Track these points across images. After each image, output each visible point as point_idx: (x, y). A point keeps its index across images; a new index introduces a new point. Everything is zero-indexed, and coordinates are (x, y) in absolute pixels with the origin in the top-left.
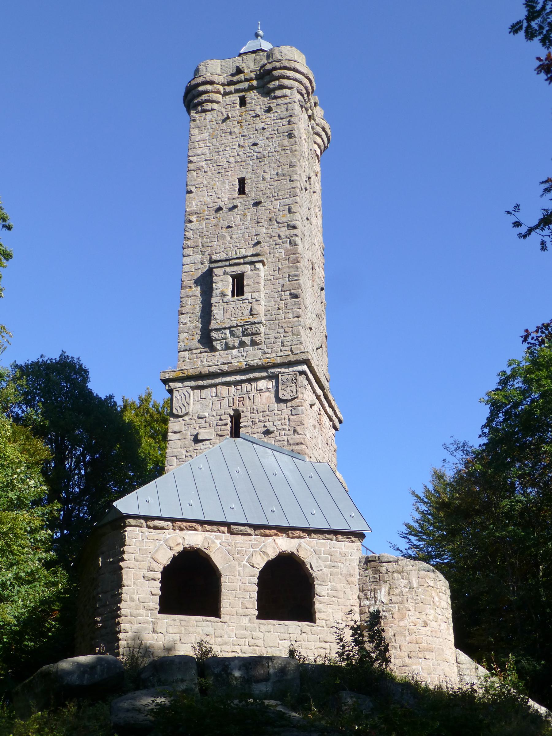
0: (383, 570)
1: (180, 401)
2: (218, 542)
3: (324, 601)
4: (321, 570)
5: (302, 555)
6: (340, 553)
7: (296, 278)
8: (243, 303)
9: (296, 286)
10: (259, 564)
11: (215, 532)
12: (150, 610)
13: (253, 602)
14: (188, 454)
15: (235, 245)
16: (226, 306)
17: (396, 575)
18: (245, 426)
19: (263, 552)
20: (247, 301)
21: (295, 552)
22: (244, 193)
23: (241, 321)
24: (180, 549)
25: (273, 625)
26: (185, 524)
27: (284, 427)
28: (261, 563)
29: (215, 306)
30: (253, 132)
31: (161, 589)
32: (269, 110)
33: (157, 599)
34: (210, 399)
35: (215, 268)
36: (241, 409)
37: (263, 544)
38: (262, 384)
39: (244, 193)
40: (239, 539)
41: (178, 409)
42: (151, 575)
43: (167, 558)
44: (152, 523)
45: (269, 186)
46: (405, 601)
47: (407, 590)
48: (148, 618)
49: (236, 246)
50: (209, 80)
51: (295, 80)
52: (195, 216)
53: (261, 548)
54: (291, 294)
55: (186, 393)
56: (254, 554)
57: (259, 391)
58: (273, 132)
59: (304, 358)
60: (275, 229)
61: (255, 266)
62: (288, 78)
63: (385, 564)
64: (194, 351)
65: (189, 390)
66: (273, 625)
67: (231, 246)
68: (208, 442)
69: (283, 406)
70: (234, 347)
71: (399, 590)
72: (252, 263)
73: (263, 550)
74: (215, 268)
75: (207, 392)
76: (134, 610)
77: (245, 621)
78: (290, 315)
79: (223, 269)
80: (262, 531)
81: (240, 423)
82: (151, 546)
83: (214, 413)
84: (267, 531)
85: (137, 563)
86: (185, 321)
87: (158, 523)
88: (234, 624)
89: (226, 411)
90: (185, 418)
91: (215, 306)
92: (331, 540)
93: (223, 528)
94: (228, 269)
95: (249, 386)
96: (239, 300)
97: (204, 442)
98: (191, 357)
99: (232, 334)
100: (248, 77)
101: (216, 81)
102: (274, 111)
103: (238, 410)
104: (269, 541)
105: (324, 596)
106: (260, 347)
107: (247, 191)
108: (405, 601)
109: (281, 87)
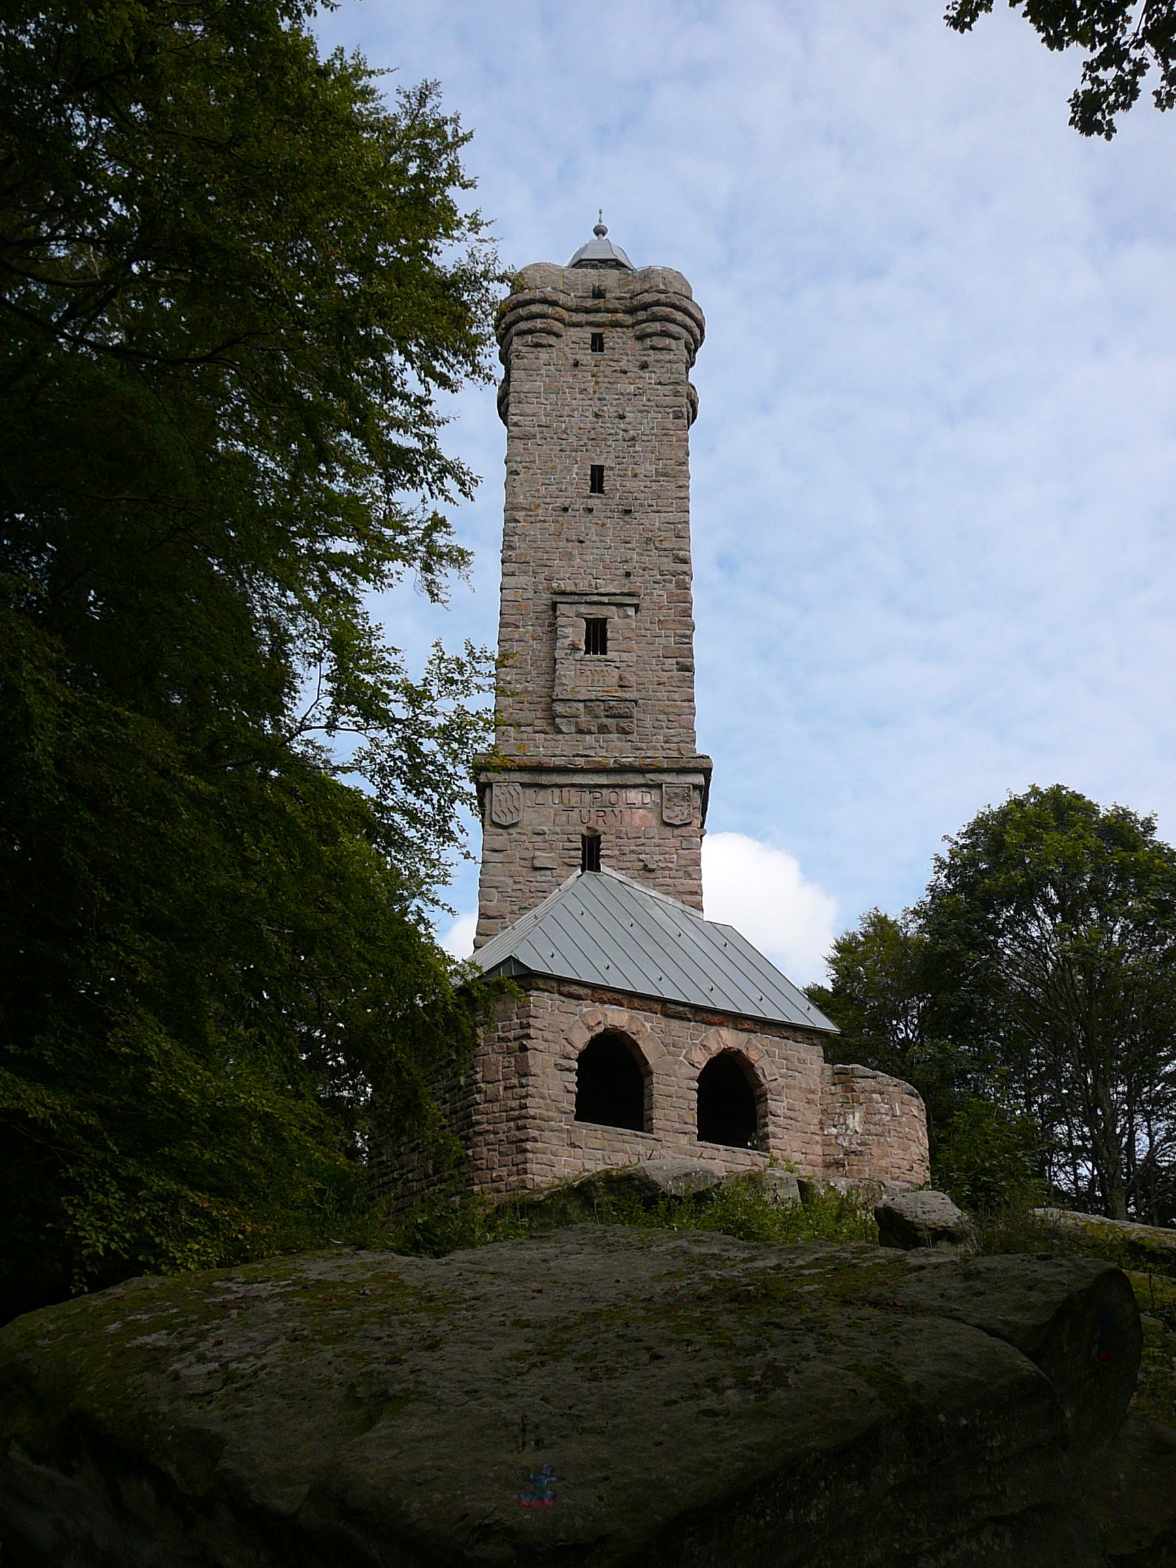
0: (857, 1086)
1: (503, 803)
2: (648, 1025)
3: (779, 1123)
4: (776, 1079)
5: (753, 1056)
6: (798, 1059)
7: (687, 641)
8: (606, 665)
9: (686, 652)
10: (700, 1063)
11: (644, 1010)
12: (565, 1113)
13: (693, 1115)
14: (518, 887)
15: (588, 571)
16: (579, 667)
17: (874, 1095)
18: (607, 856)
19: (704, 1046)
20: (613, 664)
21: (744, 1051)
22: (602, 491)
23: (604, 694)
24: (600, 1029)
25: (718, 1150)
26: (609, 995)
27: (670, 865)
28: (702, 1059)
29: (561, 663)
30: (617, 397)
31: (577, 1084)
32: (644, 366)
33: (573, 1097)
34: (552, 807)
35: (561, 603)
36: (600, 829)
37: (704, 1034)
38: (634, 796)
39: (602, 491)
40: (675, 1024)
41: (500, 814)
42: (565, 1063)
43: (585, 1041)
44: (566, 989)
45: (642, 488)
46: (887, 1134)
47: (889, 1118)
48: (562, 1124)
49: (590, 574)
50: (550, 299)
51: (685, 327)
52: (523, 513)
53: (702, 1040)
54: (677, 663)
55: (513, 792)
56: (693, 1047)
57: (631, 806)
58: (648, 403)
59: (705, 766)
60: (653, 558)
61: (625, 611)
62: (674, 321)
63: (859, 1080)
64: (523, 729)
65: (519, 788)
66: (718, 1150)
67: (582, 571)
68: (548, 872)
69: (668, 832)
70: (590, 733)
71: (878, 1117)
72: (620, 605)
73: (704, 1043)
74: (561, 603)
75: (544, 796)
76: (544, 1112)
77: (684, 1140)
78: (676, 696)
79: (574, 606)
80: (704, 1015)
81: (600, 850)
82: (563, 1021)
83: (558, 829)
84: (711, 1018)
85: (546, 1045)
86: (508, 679)
87: (573, 989)
88: (669, 1145)
89: (577, 828)
90: (511, 831)
91: (561, 663)
92: (787, 1038)
93: (656, 1006)
94: (583, 609)
95: (613, 797)
96: (599, 660)
97: (543, 872)
98: (519, 736)
99: (589, 711)
100: (610, 306)
101: (561, 302)
102: (650, 369)
103: (596, 831)
104: (712, 1031)
105: (779, 1116)
106: (629, 737)
107: (606, 487)
108: (887, 1134)
109: (665, 334)
